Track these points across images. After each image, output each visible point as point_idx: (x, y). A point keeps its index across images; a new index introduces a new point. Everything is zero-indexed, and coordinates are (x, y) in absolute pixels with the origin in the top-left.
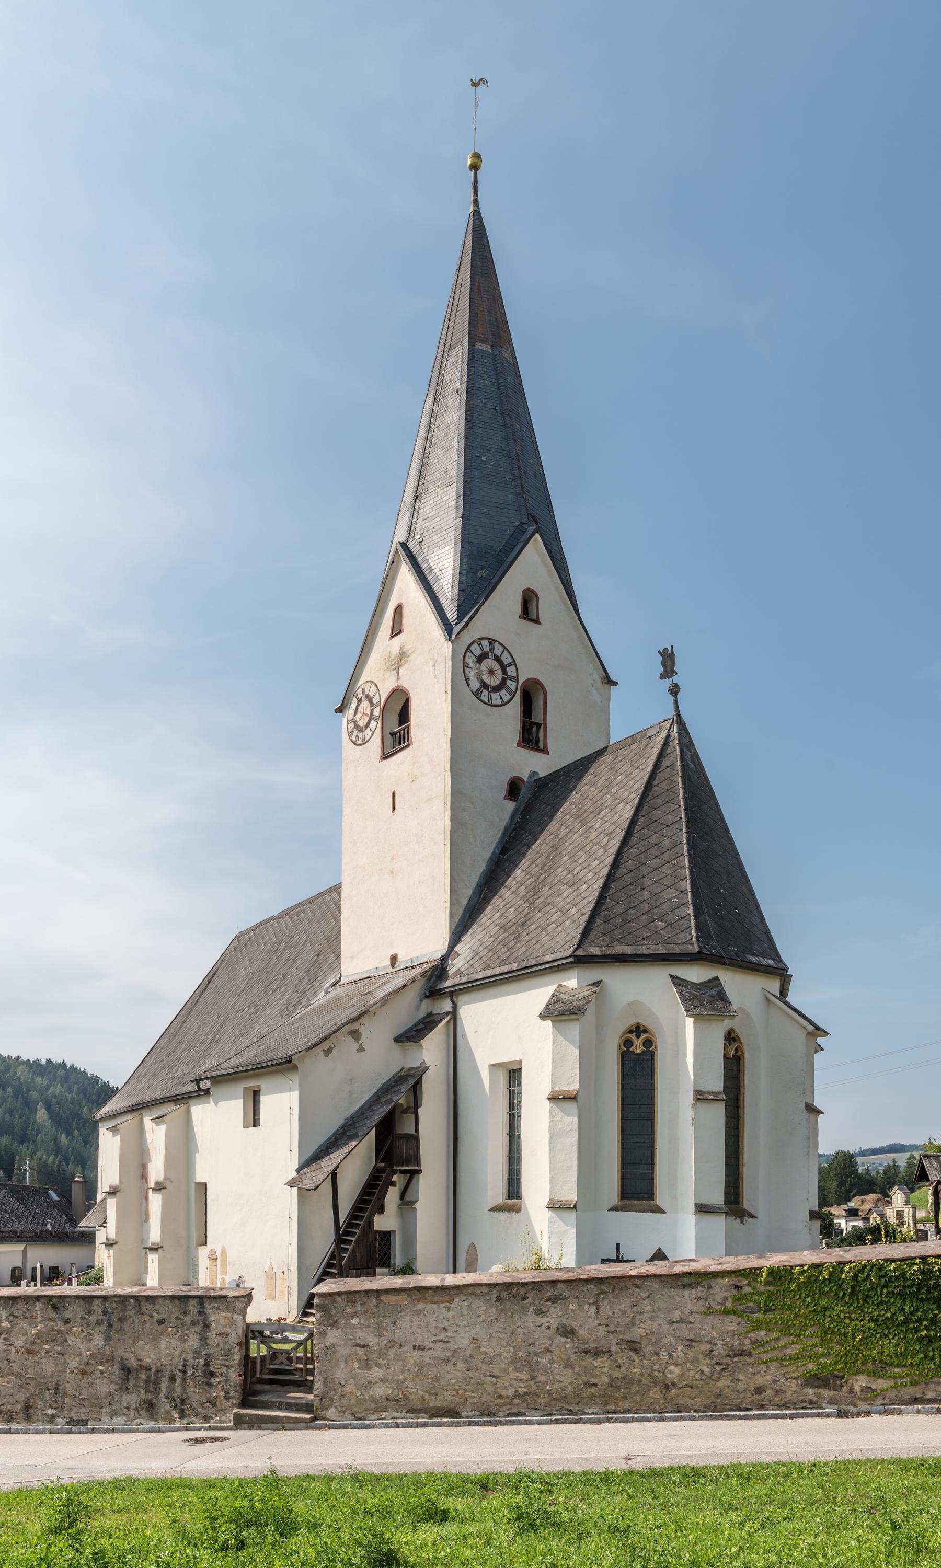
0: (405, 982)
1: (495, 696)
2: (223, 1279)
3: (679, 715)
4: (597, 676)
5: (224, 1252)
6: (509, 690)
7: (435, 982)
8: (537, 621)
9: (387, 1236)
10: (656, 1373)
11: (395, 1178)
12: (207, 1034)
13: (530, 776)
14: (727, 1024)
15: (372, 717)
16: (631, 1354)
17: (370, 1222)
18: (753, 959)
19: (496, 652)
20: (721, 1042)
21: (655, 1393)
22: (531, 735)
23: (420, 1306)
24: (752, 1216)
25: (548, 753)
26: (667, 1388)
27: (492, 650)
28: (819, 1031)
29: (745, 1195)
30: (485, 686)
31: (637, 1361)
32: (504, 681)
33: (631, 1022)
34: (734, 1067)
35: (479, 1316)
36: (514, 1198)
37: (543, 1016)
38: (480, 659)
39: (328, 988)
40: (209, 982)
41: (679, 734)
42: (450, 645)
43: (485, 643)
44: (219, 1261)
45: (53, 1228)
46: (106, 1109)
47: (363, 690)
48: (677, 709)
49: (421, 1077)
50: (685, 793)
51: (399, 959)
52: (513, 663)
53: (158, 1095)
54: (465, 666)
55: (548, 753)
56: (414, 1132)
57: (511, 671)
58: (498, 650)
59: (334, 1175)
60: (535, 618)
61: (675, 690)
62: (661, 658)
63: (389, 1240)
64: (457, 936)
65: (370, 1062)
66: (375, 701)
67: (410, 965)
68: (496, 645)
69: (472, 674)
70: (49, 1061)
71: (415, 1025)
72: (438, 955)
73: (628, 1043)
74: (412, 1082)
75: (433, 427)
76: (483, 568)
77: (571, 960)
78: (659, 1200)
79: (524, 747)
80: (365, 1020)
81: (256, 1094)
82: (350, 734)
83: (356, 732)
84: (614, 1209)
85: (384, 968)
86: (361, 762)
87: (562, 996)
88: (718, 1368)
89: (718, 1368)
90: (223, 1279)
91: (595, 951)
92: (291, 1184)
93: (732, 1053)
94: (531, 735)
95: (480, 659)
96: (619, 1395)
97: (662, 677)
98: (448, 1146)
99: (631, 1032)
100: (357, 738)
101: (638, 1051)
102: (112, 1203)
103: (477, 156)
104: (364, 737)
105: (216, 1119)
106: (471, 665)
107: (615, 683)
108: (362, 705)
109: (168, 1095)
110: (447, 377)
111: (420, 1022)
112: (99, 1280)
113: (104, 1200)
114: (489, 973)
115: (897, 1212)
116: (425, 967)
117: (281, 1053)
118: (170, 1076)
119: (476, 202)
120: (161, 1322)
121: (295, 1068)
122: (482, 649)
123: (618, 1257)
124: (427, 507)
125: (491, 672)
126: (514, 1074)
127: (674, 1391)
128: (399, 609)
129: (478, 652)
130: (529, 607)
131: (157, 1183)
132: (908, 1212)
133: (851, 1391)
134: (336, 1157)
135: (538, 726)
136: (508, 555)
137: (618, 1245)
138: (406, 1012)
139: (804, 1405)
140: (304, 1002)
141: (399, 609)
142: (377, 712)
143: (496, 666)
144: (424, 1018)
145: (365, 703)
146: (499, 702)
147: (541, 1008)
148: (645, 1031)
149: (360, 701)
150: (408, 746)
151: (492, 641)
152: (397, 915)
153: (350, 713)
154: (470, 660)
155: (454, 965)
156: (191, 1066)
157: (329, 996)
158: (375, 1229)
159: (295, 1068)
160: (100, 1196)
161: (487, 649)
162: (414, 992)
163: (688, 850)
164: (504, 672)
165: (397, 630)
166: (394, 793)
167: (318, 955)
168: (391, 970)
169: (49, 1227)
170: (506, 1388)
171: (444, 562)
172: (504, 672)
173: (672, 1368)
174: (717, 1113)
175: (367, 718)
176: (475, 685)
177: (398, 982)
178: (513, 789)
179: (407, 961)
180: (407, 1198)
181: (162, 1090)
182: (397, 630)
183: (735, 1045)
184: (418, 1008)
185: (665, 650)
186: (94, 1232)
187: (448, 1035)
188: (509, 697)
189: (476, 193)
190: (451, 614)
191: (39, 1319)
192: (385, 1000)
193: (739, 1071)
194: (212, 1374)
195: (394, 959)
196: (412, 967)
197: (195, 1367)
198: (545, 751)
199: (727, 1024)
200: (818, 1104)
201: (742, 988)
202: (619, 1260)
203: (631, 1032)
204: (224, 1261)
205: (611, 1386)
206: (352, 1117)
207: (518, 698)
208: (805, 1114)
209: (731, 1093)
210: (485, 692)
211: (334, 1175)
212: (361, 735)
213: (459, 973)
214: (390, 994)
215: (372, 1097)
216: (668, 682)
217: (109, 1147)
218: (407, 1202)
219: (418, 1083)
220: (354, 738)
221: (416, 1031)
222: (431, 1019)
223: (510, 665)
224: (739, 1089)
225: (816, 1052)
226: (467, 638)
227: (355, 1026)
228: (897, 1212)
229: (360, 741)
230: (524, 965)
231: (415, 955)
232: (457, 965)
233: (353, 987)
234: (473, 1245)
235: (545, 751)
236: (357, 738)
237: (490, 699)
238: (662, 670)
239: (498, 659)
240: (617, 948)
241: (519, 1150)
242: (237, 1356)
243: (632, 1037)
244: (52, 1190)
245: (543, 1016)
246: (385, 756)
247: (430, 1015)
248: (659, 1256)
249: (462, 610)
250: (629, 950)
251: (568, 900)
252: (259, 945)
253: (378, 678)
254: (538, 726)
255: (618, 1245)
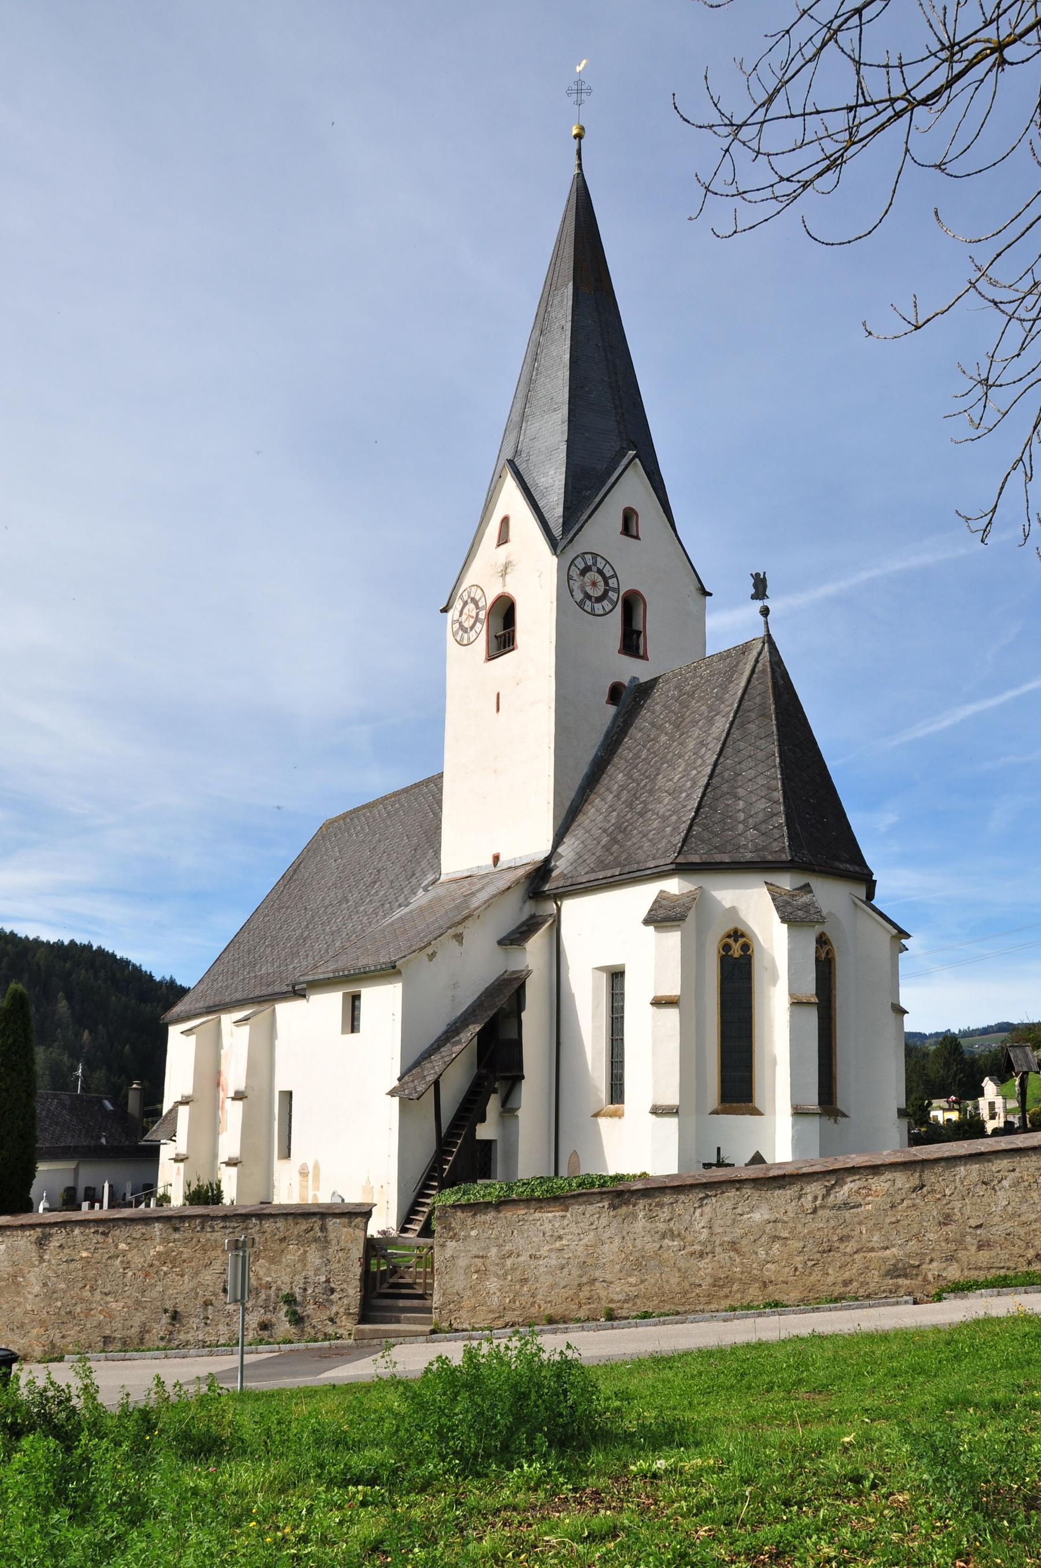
0: (509, 884)
1: (597, 606)
2: (315, 1196)
3: (769, 635)
4: (693, 586)
5: (316, 1166)
6: (611, 601)
7: (539, 884)
8: (637, 537)
9: (488, 1144)
10: (755, 1272)
11: (497, 1085)
12: (294, 930)
13: (630, 682)
14: (818, 929)
15: (477, 619)
16: (732, 1254)
17: (473, 1131)
18: (841, 866)
19: (598, 565)
20: (814, 945)
21: (754, 1292)
22: (632, 643)
23: (537, 1215)
24: (844, 1115)
25: (647, 659)
26: (765, 1285)
27: (595, 564)
28: (903, 934)
29: (838, 1096)
30: (588, 596)
31: (738, 1260)
32: (606, 592)
33: (729, 927)
34: (825, 970)
35: (592, 1224)
36: (618, 1103)
37: (647, 922)
38: (584, 572)
39: (428, 886)
40: (295, 871)
41: (770, 653)
42: (555, 559)
43: (588, 557)
44: (310, 1176)
45: (107, 1142)
46: (178, 1009)
47: (469, 593)
48: (768, 631)
49: (524, 982)
50: (776, 709)
51: (501, 859)
52: (615, 576)
53: (238, 996)
54: (569, 578)
55: (647, 659)
56: (515, 1036)
57: (613, 583)
58: (600, 564)
59: (436, 1084)
60: (635, 534)
61: (765, 612)
62: (753, 581)
63: (490, 1150)
64: (558, 839)
65: (472, 966)
66: (481, 604)
67: (513, 865)
68: (599, 559)
69: (576, 586)
70: (72, 942)
71: (519, 927)
72: (542, 856)
73: (727, 947)
74: (516, 986)
75: (539, 357)
76: (585, 487)
77: (673, 866)
78: (758, 1103)
79: (625, 654)
80: (469, 923)
81: (356, 998)
82: (454, 634)
83: (461, 632)
84: (715, 1112)
85: (486, 867)
86: (466, 660)
87: (664, 902)
88: (810, 1264)
89: (810, 1264)
90: (315, 1196)
91: (696, 859)
92: (392, 1093)
93: (823, 956)
94: (632, 643)
95: (584, 572)
96: (722, 1293)
97: (753, 597)
98: (551, 1051)
99: (729, 936)
100: (462, 637)
101: (736, 955)
102: (184, 1112)
103: (582, 128)
104: (469, 638)
105: (308, 1021)
106: (575, 577)
107: (710, 594)
108: (467, 607)
109: (251, 996)
110: (553, 314)
111: (523, 924)
112: (217, 1198)
113: (173, 1111)
114: (593, 876)
115: (990, 1103)
116: (528, 868)
117: (384, 959)
118: (252, 975)
119: (580, 166)
120: (283, 1240)
121: (399, 973)
122: (586, 563)
123: (718, 1161)
124: (532, 427)
125: (594, 584)
126: (616, 976)
127: (771, 1288)
128: (505, 521)
129: (582, 566)
130: (629, 518)
131: (236, 1093)
132: (999, 1102)
133: (925, 1279)
134: (437, 1063)
135: (639, 633)
136: (610, 475)
137: (719, 1149)
138: (511, 914)
139: (884, 1295)
140: (401, 899)
141: (505, 521)
142: (482, 615)
143: (600, 579)
144: (528, 920)
145: (471, 606)
146: (601, 612)
147: (644, 913)
148: (743, 935)
149: (465, 603)
150: (513, 650)
151: (595, 556)
152: (500, 810)
153: (453, 614)
154: (575, 573)
155: (556, 867)
156: (276, 965)
157: (431, 895)
158: (477, 1138)
159: (399, 973)
160: (167, 1106)
161: (590, 563)
162: (517, 894)
163: (780, 763)
164: (606, 584)
165: (503, 539)
166: (498, 694)
167: (415, 850)
168: (492, 869)
169: (103, 1141)
170: (617, 1293)
171: (552, 481)
172: (606, 584)
173: (769, 1266)
174: (812, 1018)
175: (472, 621)
176: (579, 596)
177: (502, 884)
178: (616, 693)
179: (510, 861)
180: (508, 1106)
181: (243, 991)
182: (503, 539)
183: (826, 948)
184: (521, 909)
185: (758, 574)
186: (159, 1147)
187: (551, 938)
188: (611, 607)
189: (580, 158)
190: (557, 531)
191: (158, 1240)
192: (488, 903)
193: (830, 973)
194: (332, 1291)
195: (496, 859)
196: (516, 868)
197: (316, 1285)
198: (645, 657)
199: (818, 929)
200: (903, 1004)
201: (831, 895)
202: (720, 1164)
203: (729, 936)
204: (317, 1176)
205: (715, 1286)
206: (455, 1022)
207: (619, 608)
208: (892, 1015)
209: (823, 1001)
210: (588, 603)
211: (436, 1084)
212: (466, 635)
213: (563, 875)
214: (494, 896)
215: (475, 1002)
216: (759, 604)
217: (181, 1049)
218: (508, 1110)
219: (522, 987)
220: (458, 639)
221: (520, 933)
222: (534, 921)
223: (612, 577)
224: (831, 991)
225: (901, 952)
226: (571, 553)
227: (459, 929)
228: (990, 1103)
229: (465, 642)
230: (626, 870)
231: (517, 855)
232: (561, 866)
233: (454, 886)
234: (575, 1152)
235: (645, 657)
236: (462, 637)
237: (593, 609)
238: (753, 591)
239: (600, 572)
240: (715, 856)
241: (622, 1054)
242: (358, 1270)
243: (731, 941)
244: (106, 1099)
245: (647, 922)
246: (490, 658)
247: (533, 917)
248: (758, 1159)
249: (566, 525)
250: (726, 859)
251: (669, 807)
252: (351, 835)
253: (484, 581)
254: (639, 633)
255: (719, 1149)
